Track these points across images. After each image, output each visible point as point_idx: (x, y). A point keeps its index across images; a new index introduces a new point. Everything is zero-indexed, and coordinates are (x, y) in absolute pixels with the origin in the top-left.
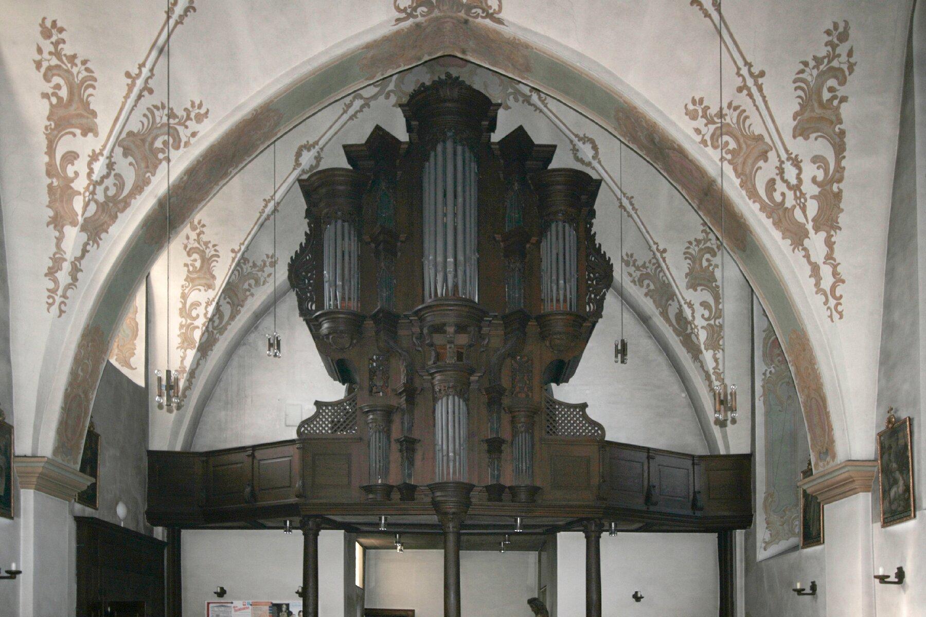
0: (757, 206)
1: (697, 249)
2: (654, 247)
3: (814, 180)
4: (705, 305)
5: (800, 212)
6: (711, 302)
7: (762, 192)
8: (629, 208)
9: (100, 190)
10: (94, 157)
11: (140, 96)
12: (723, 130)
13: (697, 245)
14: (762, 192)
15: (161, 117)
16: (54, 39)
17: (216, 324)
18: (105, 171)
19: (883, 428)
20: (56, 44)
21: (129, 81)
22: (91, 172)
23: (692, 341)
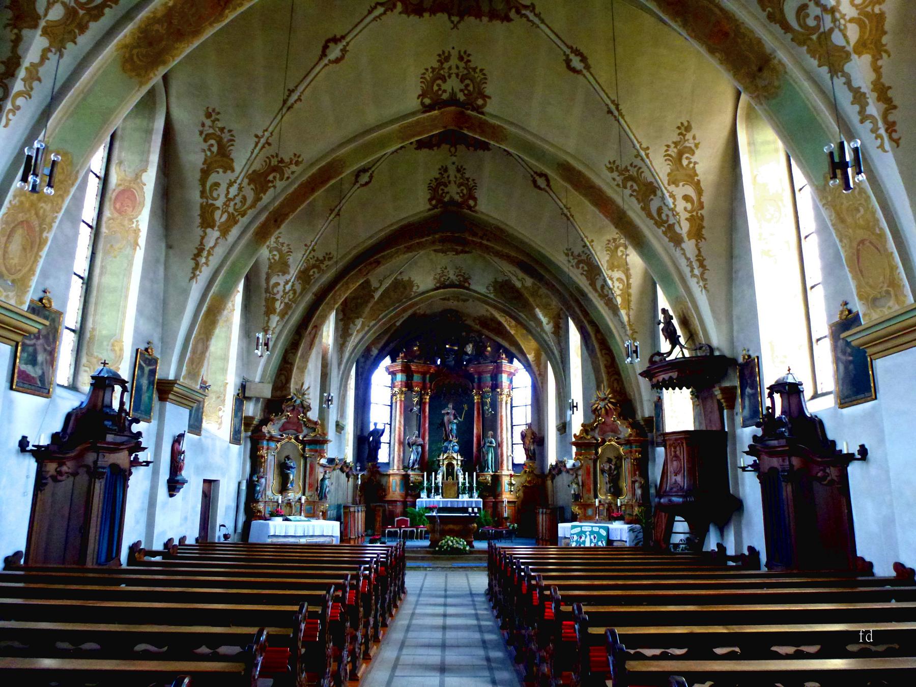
0: (653, 222)
1: (675, 150)
2: (638, 146)
3: (685, 209)
4: (686, 198)
5: (840, 34)
6: (624, 278)
7: (655, 215)
8: (616, 113)
9: (232, 204)
10: (231, 184)
11: (263, 147)
12: (579, 262)
13: (676, 147)
14: (655, 215)
15: (274, 162)
16: (213, 118)
17: (237, 207)
18: (236, 193)
19: (837, 319)
20: (213, 122)
21: (257, 140)
22: (228, 193)
23: (675, 232)
